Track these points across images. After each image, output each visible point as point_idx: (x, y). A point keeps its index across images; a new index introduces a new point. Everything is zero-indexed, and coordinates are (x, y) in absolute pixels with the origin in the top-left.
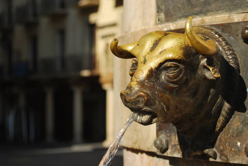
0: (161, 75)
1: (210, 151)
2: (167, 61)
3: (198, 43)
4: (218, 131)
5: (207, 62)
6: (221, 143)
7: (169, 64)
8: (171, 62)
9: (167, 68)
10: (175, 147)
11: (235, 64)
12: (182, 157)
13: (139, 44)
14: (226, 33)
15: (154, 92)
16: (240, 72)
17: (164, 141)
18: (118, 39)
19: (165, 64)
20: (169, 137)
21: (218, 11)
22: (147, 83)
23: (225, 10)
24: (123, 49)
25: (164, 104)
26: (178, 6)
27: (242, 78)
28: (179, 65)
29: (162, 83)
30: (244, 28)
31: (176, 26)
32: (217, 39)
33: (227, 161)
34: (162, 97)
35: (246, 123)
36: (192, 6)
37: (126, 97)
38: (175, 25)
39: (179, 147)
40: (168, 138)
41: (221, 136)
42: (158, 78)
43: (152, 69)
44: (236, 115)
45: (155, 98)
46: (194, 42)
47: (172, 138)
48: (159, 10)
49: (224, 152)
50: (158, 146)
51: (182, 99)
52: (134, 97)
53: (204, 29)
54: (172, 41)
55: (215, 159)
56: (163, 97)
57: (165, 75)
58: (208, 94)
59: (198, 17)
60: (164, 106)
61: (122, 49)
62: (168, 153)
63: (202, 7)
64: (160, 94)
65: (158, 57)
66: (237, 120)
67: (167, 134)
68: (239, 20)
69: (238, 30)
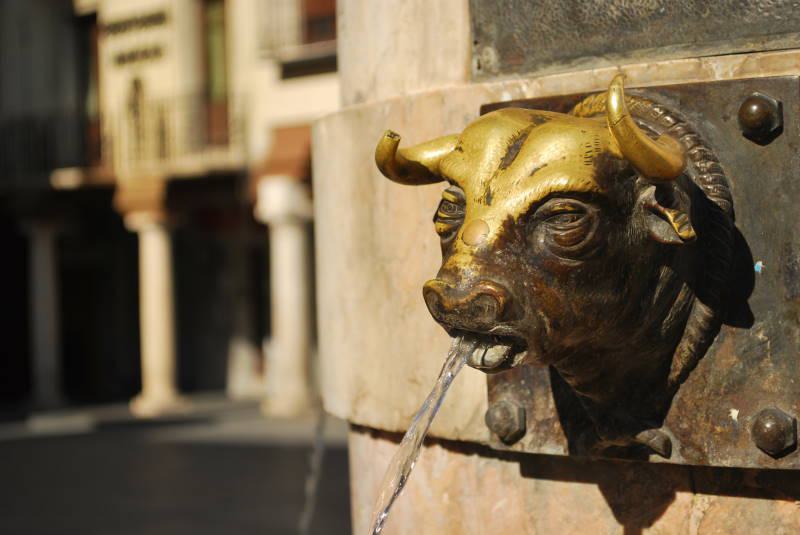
0: (535, 233)
1: (655, 435)
2: (552, 195)
3: (643, 147)
4: (675, 379)
5: (657, 195)
6: (683, 413)
7: (556, 204)
8: (563, 197)
9: (552, 216)
10: (546, 428)
11: (723, 198)
12: (567, 454)
13: (463, 147)
14: (693, 109)
15: (519, 283)
16: (734, 220)
17: (514, 410)
18: (398, 133)
19: (548, 204)
20: (527, 398)
21: (662, 45)
22: (501, 257)
23: (683, 45)
24: (407, 158)
25: (547, 313)
26: (539, 30)
27: (741, 235)
28: (584, 205)
29: (538, 257)
30: (744, 99)
31: (539, 86)
32: (670, 130)
33: (700, 461)
34: (540, 294)
35: (754, 356)
36: (584, 30)
37: (445, 298)
38: (535, 83)
39: (557, 425)
40: (525, 401)
41: (685, 395)
42: (527, 243)
43: (510, 218)
44: (724, 335)
45: (524, 298)
46: (631, 146)
47: (537, 402)
48: (478, 36)
49: (694, 436)
50: (496, 426)
51: (590, 299)
52: (468, 298)
53: (632, 101)
54: (563, 139)
55: (668, 455)
56: (543, 295)
57: (547, 235)
58: (654, 281)
59: (603, 61)
60: (546, 319)
61: (405, 159)
62: (527, 444)
63: (613, 35)
64: (536, 286)
65: (525, 185)
66: (726, 352)
67: (522, 391)
68: (726, 74)
69: (727, 104)
